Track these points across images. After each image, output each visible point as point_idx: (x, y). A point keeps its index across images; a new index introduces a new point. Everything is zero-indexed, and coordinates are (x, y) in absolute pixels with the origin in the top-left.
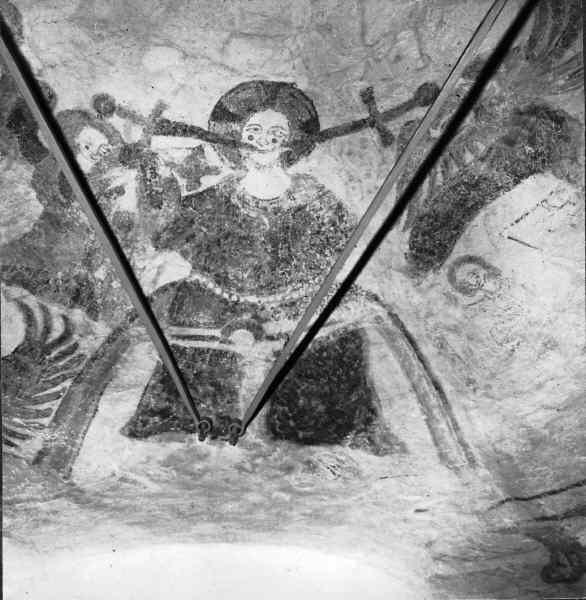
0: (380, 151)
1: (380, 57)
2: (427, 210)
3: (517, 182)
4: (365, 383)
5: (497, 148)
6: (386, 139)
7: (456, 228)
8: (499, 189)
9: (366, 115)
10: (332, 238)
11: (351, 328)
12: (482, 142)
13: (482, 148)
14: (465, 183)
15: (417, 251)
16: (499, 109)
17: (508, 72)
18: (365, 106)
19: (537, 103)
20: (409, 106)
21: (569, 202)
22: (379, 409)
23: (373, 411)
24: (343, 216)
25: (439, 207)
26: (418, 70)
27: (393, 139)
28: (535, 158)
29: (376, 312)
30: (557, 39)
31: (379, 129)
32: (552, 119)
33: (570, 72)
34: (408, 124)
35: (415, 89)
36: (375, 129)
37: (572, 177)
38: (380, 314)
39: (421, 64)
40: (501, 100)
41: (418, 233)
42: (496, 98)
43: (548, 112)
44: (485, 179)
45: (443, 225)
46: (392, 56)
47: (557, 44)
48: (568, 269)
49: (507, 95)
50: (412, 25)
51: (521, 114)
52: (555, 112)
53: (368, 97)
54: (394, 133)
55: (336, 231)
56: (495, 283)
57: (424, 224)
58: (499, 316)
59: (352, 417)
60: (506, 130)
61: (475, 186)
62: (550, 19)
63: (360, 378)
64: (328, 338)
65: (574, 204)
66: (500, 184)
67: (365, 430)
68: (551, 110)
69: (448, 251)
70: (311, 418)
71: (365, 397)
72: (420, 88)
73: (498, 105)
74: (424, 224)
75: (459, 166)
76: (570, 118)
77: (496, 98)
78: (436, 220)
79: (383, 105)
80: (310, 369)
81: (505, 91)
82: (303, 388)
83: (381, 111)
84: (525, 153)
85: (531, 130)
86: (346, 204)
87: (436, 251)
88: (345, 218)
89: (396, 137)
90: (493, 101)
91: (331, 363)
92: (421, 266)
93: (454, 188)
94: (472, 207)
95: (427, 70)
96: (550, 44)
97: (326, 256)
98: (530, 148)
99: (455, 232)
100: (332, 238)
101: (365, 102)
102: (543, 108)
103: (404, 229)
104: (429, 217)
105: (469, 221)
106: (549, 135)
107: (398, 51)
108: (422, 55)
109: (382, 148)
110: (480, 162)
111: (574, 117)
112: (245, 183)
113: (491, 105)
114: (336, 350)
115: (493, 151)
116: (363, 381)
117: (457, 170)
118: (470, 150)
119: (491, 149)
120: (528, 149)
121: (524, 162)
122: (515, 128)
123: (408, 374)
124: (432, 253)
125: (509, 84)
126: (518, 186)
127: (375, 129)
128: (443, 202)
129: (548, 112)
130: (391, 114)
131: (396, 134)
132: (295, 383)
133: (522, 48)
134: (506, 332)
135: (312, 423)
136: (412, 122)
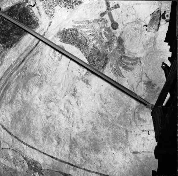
0: (99, 13)
1: (129, 10)
2: (79, 32)
3: (86, 58)
4: (20, 37)
5: (97, 50)
6: (102, 14)
7: (73, 43)
8: (85, 53)
9: (111, 7)
10: (70, 2)
11: (39, 22)
12: (99, 45)
13: (97, 45)
14: (87, 42)
15: (66, 32)
16: (108, 49)
17: (118, 51)
18: (114, 6)
19: (108, 60)
20: (112, 20)
21: (81, 74)
22: (13, 47)
23: (12, 46)
24: (78, 4)
25: (80, 36)
26: (123, 23)
27: (102, 17)
28: (93, 62)
29: (45, 28)
30: (126, 64)
31: (106, 12)
32: (104, 65)
33: (116, 68)
34: (107, 21)
35: (117, 22)
36: (106, 10)
37: (88, 73)
38: (45, 29)
39: (124, 23)
40: (110, 50)
41: (72, 31)
42: (111, 48)
43: (106, 64)
44: (88, 48)
45: (74, 38)
46: (129, 14)
47: (124, 64)
48: (62, 81)
49: (112, 51)
50: (137, 20)
51: (106, 56)
52: (106, 66)
53: (117, 6)
54: (104, 17)
55: (72, 3)
56: (57, 60)
57: (74, 32)
58: (47, 88)
59: (9, 40)
60: (102, 52)
61: (86, 45)
62: (131, 62)
63: (22, 34)
64: (35, 16)
65: (80, 76)
66: (86, 53)
67: (4, 48)
68: (106, 64)
69: (66, 42)
70: (5, 28)
71: (16, 40)
72: (117, 23)
73: (109, 49)
74: (74, 32)
75: (92, 39)
76: (104, 70)
77: (111, 48)
78: (76, 35)
79: (113, 12)
80: (23, 17)
81: (113, 50)
82: (15, 18)
83: (112, 12)
84: (94, 59)
85: (101, 59)
86: (82, 5)
87: (66, 38)
88: (77, 5)
89: (103, 18)
90: (111, 47)
91: (26, 22)
92: (61, 35)
93: (86, 39)
94: (80, 46)
95: (122, 25)
96: (125, 63)
97: (64, 2)
98: (96, 59)
99: (72, 43)
100: (70, 2)
101: (115, 6)
102: (107, 62)
103: (73, 26)
104: (77, 33)
105: (75, 46)
106: (100, 65)
107: (130, 16)
108: (127, 23)
109: (100, 14)
110: (93, 45)
111: (104, 71)
112: (94, 175)
113: (109, 47)
114: (31, 21)
115: (96, 49)
116: (20, 36)
117: (91, 39)
118: (97, 42)
119: (97, 48)
120: (96, 59)
121: (92, 58)
122: (102, 55)
123: (26, 50)
124: (65, 37)
125: (115, 52)
126: (85, 58)
127: (106, 10)
128: (82, 36)
129: (106, 64)
130: (110, 15)
131: (104, 17)
132: (16, 14)
133: (125, 54)
134: (42, 70)
135: (3, 29)
136: (107, 22)
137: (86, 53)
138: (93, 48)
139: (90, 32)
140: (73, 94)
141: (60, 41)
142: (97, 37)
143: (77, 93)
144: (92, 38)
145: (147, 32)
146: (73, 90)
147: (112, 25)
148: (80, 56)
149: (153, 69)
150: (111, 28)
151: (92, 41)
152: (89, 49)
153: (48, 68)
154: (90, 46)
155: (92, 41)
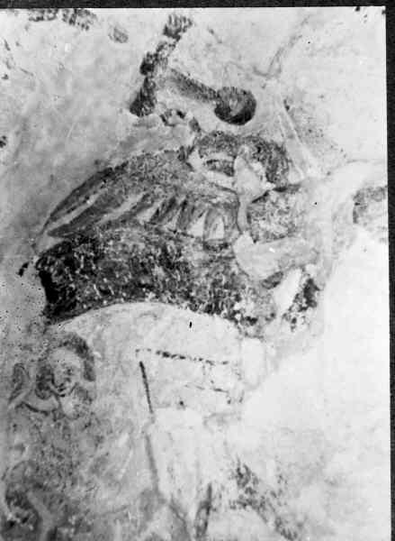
8: (188, 297)
14: (165, 250)
44: (187, 271)
61: (169, 265)
66: (193, 294)
110: (200, 247)
137: (193, 294)
138: (208, 258)
139: (149, 206)
140: (241, 497)
141: (284, 320)
142: (190, 203)
143: (12, 485)
144: (175, 220)
145: (26, 33)
146: (234, 482)
147: (222, 113)
148: (275, 325)
149: (204, 179)
150: (225, 127)
151: (184, 234)
152: (196, 272)
153: (55, 461)
154: (189, 258)
155: (184, 234)
